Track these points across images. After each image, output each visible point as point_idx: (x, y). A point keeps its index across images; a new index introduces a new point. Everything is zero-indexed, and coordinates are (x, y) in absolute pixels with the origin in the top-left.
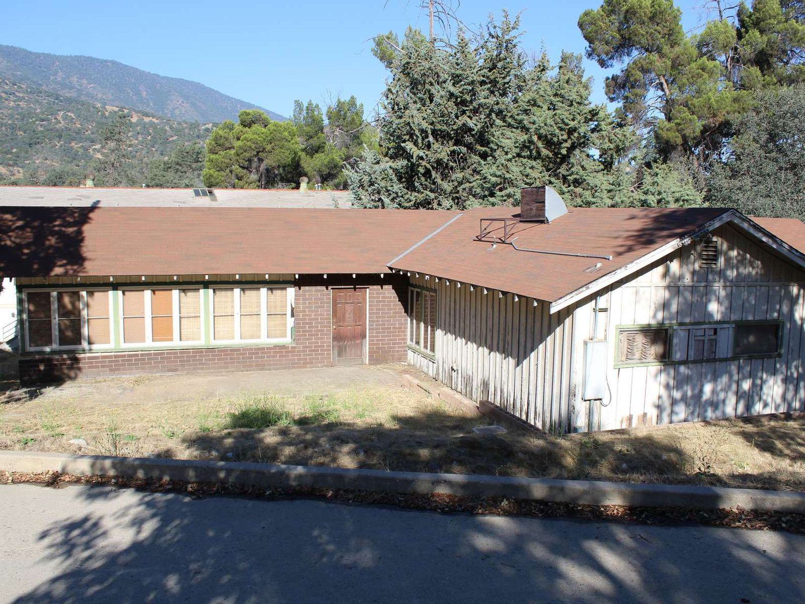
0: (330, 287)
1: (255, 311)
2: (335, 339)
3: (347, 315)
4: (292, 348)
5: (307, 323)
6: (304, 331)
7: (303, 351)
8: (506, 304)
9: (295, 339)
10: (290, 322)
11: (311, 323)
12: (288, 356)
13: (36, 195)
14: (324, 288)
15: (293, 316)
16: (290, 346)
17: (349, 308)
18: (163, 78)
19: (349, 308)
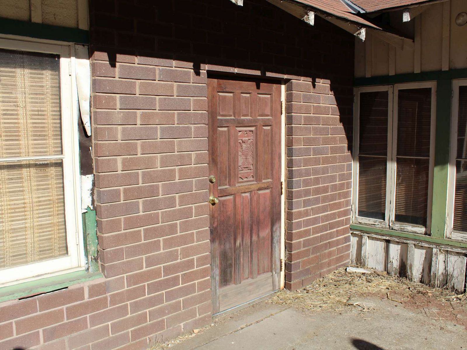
0: (205, 68)
1: (53, 158)
2: (215, 234)
3: (241, 161)
4: (95, 290)
5: (140, 193)
6: (131, 223)
7: (131, 295)
8: (21, 255)
9: (99, 258)
10: (78, 189)
11: (153, 191)
12: (82, 324)
13: (247, 92)
14: (188, 67)
15: (86, 167)
16: (86, 284)
17: (245, 136)
18: (426, 255)
19: (245, 136)
